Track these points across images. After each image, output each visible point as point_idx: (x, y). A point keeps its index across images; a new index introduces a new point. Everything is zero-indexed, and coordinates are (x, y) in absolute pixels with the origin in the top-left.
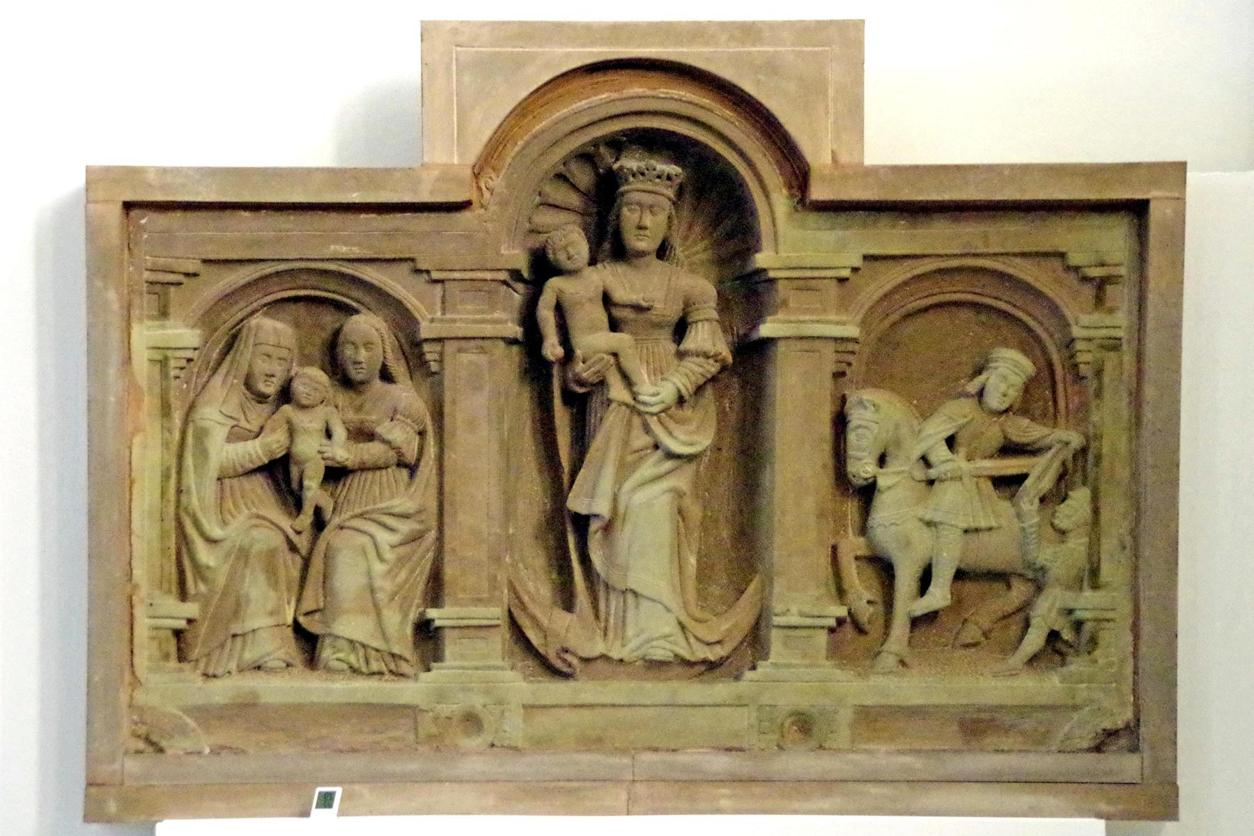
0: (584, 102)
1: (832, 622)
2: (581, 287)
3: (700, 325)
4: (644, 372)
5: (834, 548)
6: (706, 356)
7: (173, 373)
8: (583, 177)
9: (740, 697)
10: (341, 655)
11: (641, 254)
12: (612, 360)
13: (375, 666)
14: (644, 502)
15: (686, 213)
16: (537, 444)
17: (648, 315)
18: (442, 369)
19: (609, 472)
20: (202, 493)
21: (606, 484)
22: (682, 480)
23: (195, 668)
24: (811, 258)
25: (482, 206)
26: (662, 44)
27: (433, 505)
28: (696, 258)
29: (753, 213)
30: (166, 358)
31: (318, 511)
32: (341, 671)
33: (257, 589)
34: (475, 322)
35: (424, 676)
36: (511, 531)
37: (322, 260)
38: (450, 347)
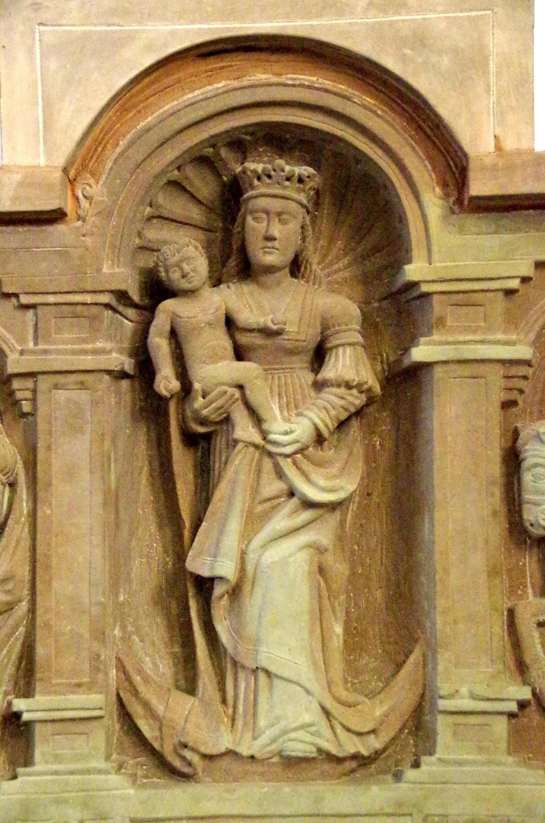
0: (197, 92)
1: (513, 707)
2: (202, 309)
3: (341, 350)
4: (276, 408)
5: (511, 612)
6: (348, 386)
8: (205, 186)
9: (400, 805)
11: (270, 270)
12: (237, 394)
14: (278, 565)
15: (325, 224)
16: (154, 492)
17: (279, 340)
19: (235, 525)
21: (231, 541)
22: (323, 533)
24: (469, 266)
25: (79, 218)
26: (287, 16)
27: (24, 572)
28: (339, 276)
29: (402, 219)
34: (74, 353)
36: (122, 598)
38: (44, 383)
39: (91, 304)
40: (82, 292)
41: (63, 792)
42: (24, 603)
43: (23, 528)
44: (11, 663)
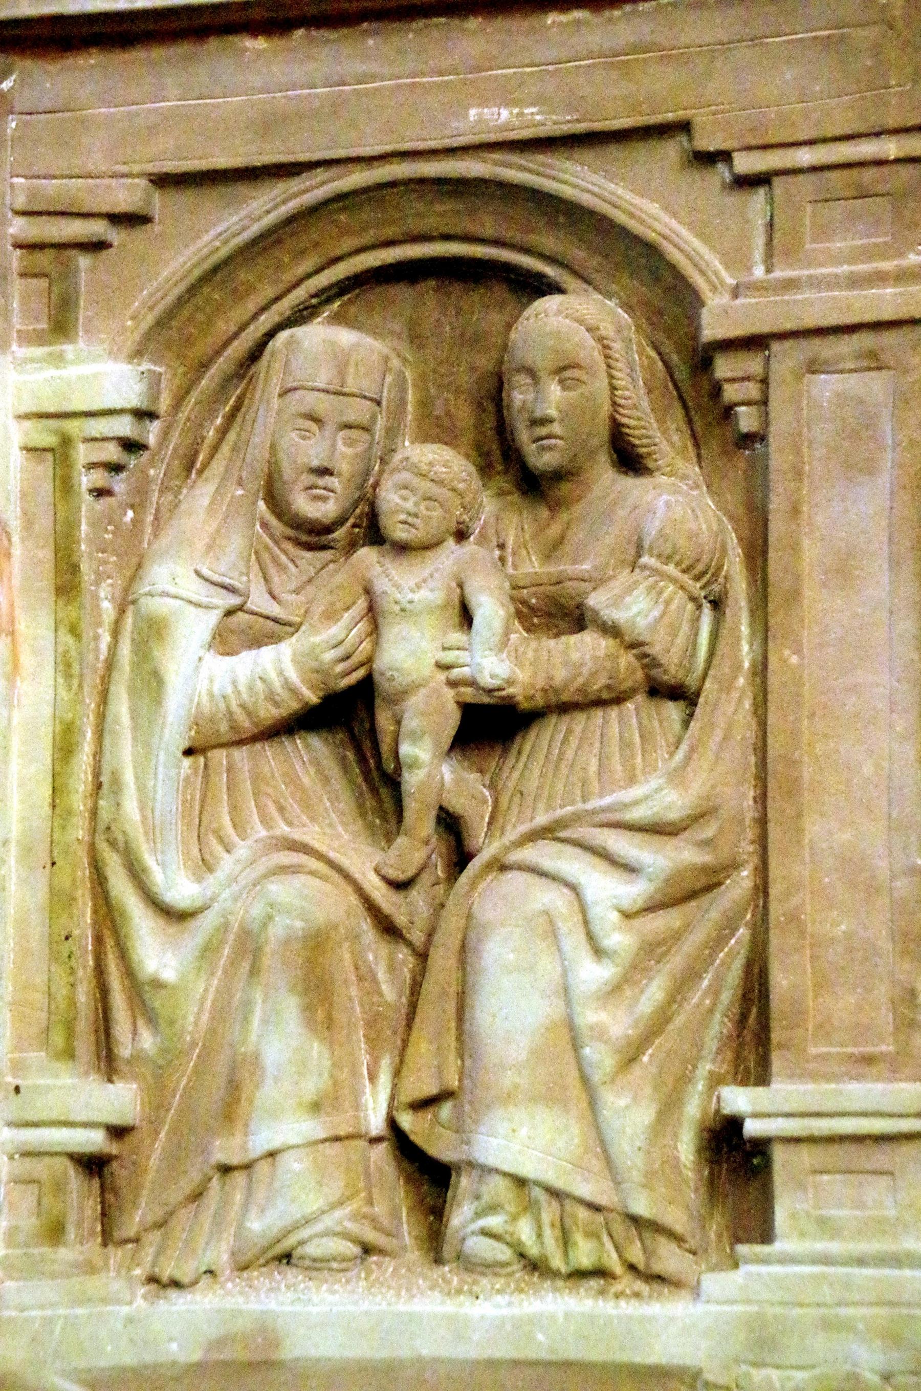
7: (86, 481)
10: (494, 1222)
13: (584, 1254)
18: (766, 422)
20: (151, 785)
23: (135, 1260)
27: (745, 800)
30: (66, 441)
31: (450, 824)
32: (491, 1267)
33: (282, 1043)
34: (855, 281)
35: (716, 1283)
37: (450, 152)
38: (786, 359)
39: (897, 161)
40: (878, 134)
41: (839, 1304)
42: (745, 873)
43: (740, 701)
44: (721, 1008)
